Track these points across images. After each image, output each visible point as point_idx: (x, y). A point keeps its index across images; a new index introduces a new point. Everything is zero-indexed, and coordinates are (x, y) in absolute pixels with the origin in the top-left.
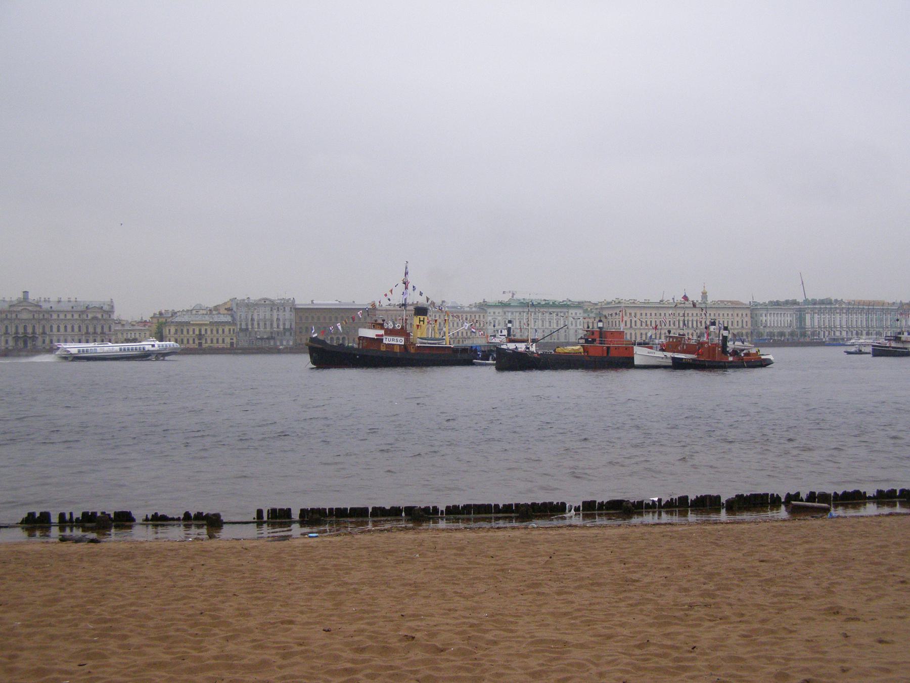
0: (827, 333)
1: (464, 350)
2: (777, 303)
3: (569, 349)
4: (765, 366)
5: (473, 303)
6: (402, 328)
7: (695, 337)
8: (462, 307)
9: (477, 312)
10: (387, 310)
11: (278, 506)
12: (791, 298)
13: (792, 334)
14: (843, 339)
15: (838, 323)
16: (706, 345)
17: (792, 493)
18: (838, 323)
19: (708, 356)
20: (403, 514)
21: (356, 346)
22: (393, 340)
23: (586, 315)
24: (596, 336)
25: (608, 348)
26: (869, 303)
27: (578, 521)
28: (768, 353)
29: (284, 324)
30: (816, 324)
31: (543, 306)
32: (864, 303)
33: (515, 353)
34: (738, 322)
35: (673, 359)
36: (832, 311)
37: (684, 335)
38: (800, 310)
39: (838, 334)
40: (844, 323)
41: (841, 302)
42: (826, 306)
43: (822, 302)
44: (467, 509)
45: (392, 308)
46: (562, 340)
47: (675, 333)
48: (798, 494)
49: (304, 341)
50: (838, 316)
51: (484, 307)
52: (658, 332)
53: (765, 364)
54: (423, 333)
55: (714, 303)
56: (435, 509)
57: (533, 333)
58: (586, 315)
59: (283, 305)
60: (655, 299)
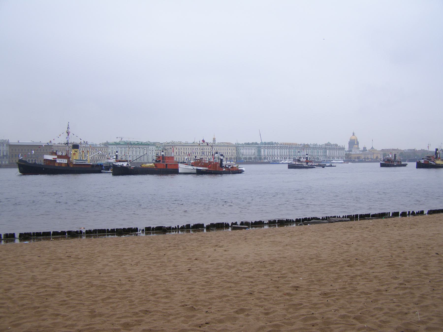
0: (271, 158)
1: (97, 165)
2: (248, 144)
3: (148, 165)
4: (240, 173)
5: (101, 142)
6: (66, 155)
7: (207, 159)
8: (96, 145)
9: (103, 147)
10: (58, 146)
11: (9, 232)
12: (254, 141)
13: (255, 158)
14: (278, 161)
15: (276, 153)
16: (212, 163)
17: (234, 222)
18: (276, 153)
19: (213, 168)
20: (67, 234)
21: (43, 164)
22: (62, 161)
23: (157, 149)
24: (161, 159)
25: (166, 164)
26: (290, 144)
27: (144, 235)
28: (242, 167)
29: (3, 153)
30: (266, 153)
31: (136, 145)
32: (288, 144)
33: (122, 167)
34: (229, 153)
35: (197, 169)
36: (273, 148)
37: (202, 158)
38: (259, 147)
39: (276, 158)
40: (279, 153)
41: (277, 144)
42: (270, 145)
43: (269, 143)
44: (95, 231)
45: (60, 145)
46: (146, 161)
47: (198, 158)
48: (236, 223)
49: (14, 161)
50: (276, 150)
51: (107, 145)
52: (190, 157)
53: (240, 172)
54: (76, 157)
55: (219, 143)
56: (81, 232)
57: (131, 157)
58: (157, 149)
59: (2, 143)
60: (190, 141)
